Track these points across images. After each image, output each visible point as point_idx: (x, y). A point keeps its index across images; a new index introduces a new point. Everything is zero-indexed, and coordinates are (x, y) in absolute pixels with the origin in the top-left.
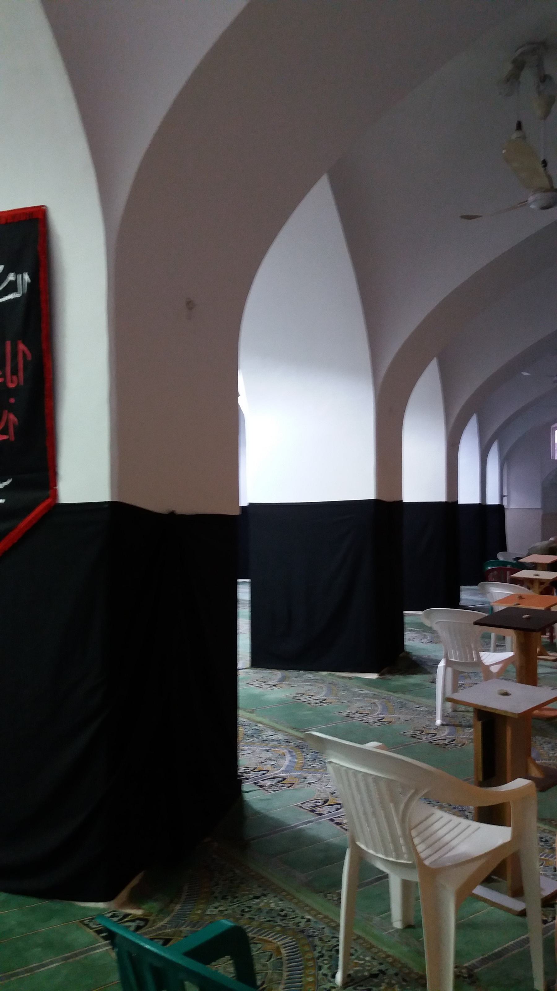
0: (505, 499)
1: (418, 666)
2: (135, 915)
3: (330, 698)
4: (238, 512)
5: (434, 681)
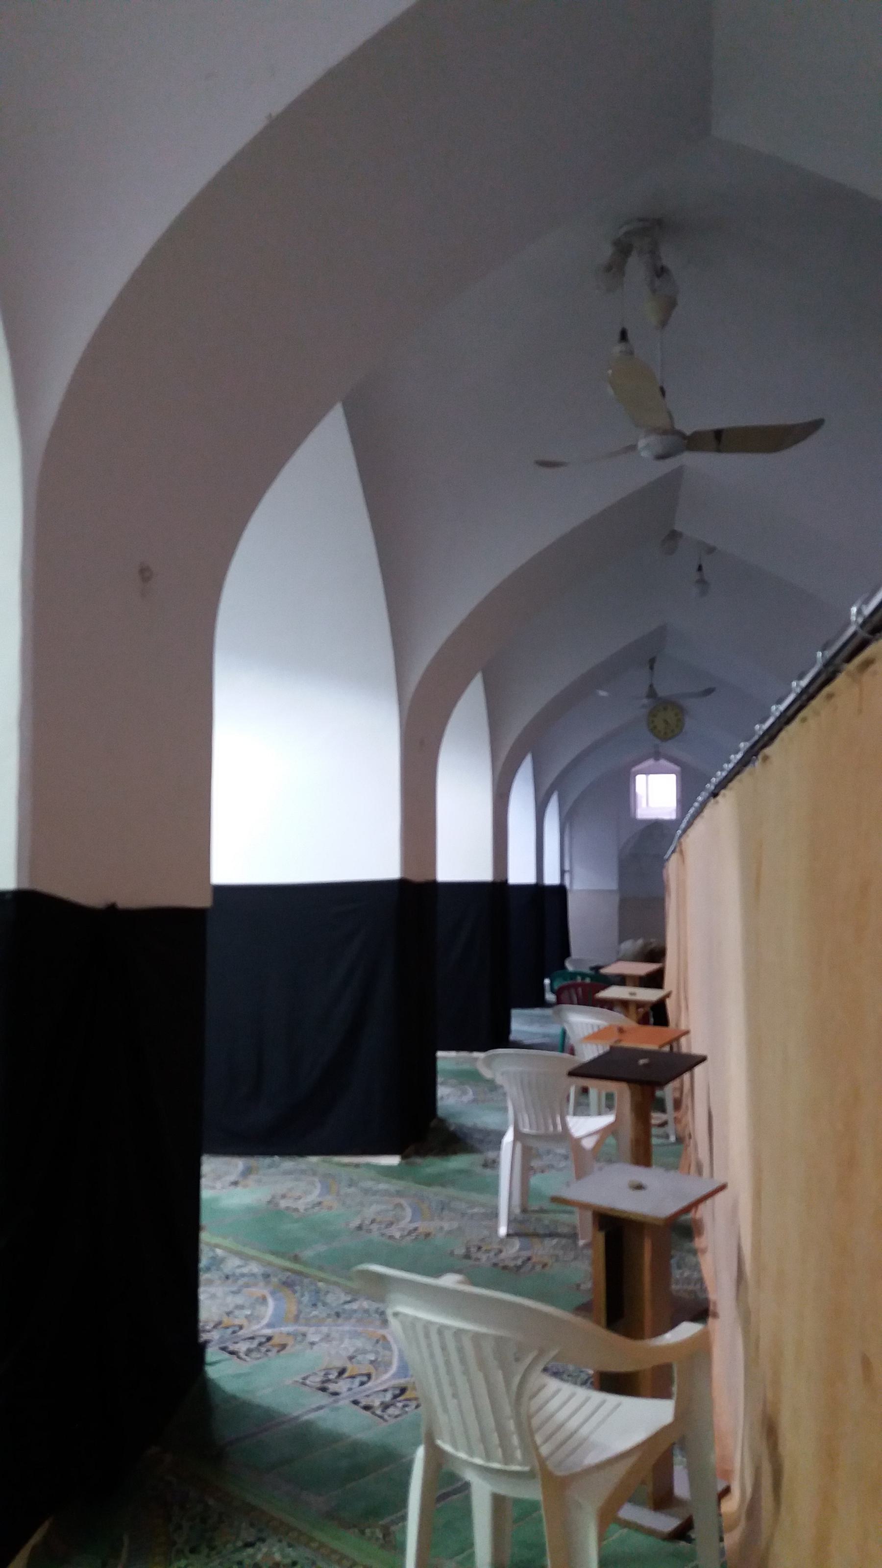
1: (451, 1140)
3: (328, 1200)
4: (204, 901)
5: (494, 1164)
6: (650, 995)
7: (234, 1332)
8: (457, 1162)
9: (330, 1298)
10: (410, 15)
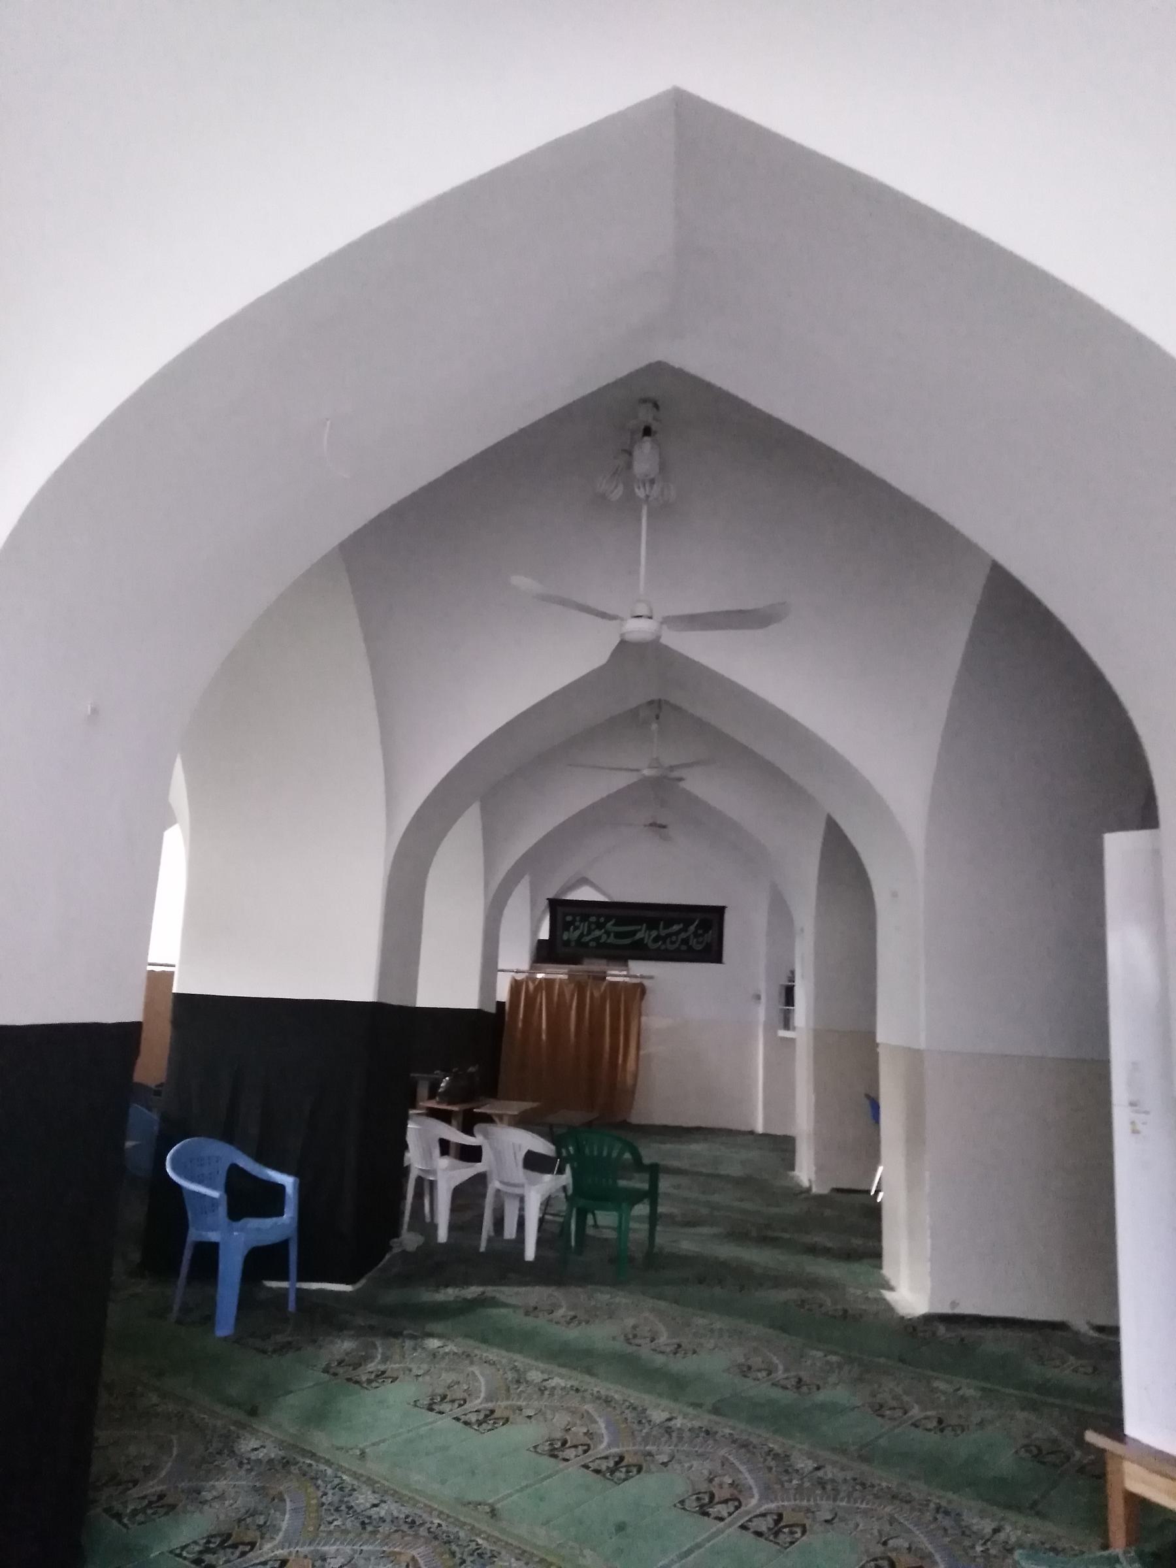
10: (1172, 359)
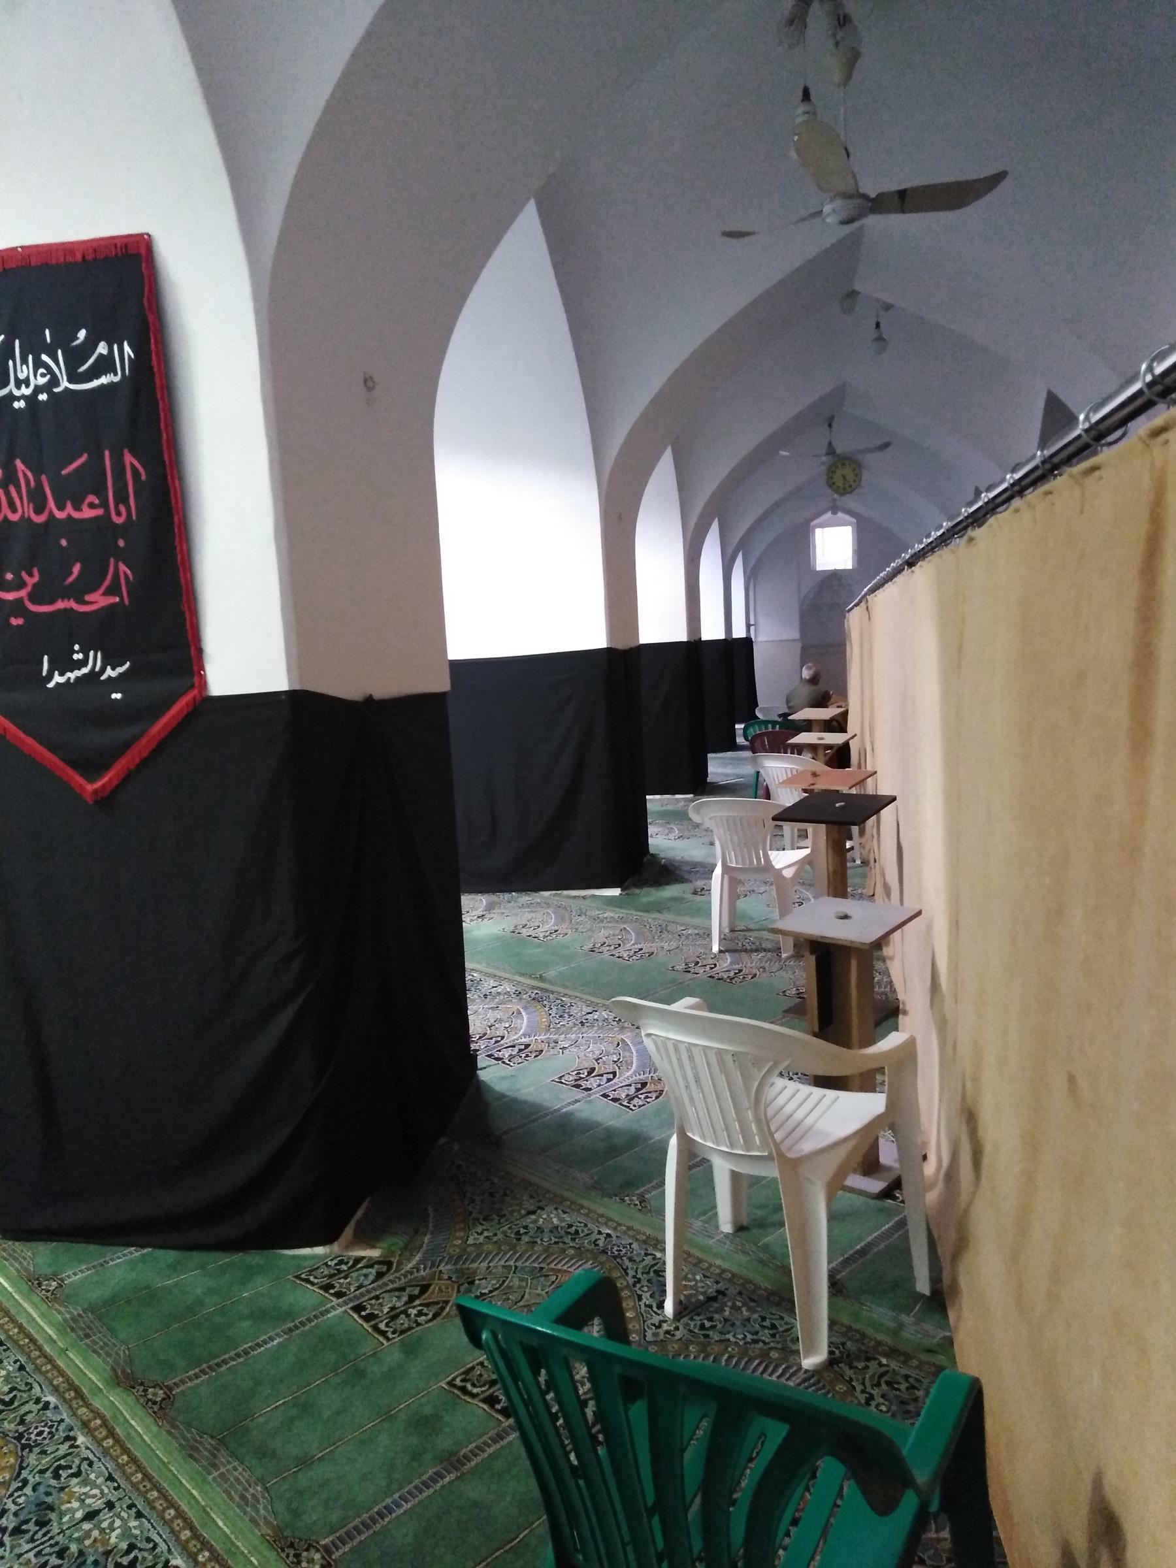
0: (752, 628)
1: (666, 873)
2: (371, 1258)
3: (563, 928)
4: (441, 683)
5: (705, 891)
6: (835, 739)
7: (497, 1042)
8: (670, 891)
9: (574, 1011)
